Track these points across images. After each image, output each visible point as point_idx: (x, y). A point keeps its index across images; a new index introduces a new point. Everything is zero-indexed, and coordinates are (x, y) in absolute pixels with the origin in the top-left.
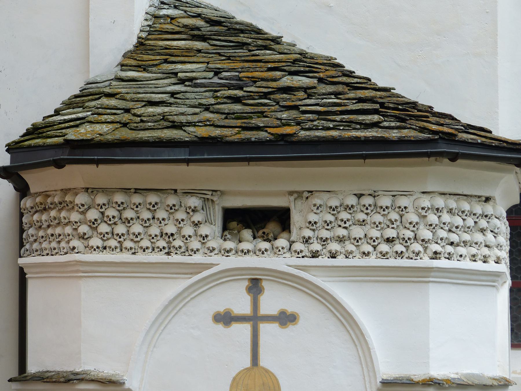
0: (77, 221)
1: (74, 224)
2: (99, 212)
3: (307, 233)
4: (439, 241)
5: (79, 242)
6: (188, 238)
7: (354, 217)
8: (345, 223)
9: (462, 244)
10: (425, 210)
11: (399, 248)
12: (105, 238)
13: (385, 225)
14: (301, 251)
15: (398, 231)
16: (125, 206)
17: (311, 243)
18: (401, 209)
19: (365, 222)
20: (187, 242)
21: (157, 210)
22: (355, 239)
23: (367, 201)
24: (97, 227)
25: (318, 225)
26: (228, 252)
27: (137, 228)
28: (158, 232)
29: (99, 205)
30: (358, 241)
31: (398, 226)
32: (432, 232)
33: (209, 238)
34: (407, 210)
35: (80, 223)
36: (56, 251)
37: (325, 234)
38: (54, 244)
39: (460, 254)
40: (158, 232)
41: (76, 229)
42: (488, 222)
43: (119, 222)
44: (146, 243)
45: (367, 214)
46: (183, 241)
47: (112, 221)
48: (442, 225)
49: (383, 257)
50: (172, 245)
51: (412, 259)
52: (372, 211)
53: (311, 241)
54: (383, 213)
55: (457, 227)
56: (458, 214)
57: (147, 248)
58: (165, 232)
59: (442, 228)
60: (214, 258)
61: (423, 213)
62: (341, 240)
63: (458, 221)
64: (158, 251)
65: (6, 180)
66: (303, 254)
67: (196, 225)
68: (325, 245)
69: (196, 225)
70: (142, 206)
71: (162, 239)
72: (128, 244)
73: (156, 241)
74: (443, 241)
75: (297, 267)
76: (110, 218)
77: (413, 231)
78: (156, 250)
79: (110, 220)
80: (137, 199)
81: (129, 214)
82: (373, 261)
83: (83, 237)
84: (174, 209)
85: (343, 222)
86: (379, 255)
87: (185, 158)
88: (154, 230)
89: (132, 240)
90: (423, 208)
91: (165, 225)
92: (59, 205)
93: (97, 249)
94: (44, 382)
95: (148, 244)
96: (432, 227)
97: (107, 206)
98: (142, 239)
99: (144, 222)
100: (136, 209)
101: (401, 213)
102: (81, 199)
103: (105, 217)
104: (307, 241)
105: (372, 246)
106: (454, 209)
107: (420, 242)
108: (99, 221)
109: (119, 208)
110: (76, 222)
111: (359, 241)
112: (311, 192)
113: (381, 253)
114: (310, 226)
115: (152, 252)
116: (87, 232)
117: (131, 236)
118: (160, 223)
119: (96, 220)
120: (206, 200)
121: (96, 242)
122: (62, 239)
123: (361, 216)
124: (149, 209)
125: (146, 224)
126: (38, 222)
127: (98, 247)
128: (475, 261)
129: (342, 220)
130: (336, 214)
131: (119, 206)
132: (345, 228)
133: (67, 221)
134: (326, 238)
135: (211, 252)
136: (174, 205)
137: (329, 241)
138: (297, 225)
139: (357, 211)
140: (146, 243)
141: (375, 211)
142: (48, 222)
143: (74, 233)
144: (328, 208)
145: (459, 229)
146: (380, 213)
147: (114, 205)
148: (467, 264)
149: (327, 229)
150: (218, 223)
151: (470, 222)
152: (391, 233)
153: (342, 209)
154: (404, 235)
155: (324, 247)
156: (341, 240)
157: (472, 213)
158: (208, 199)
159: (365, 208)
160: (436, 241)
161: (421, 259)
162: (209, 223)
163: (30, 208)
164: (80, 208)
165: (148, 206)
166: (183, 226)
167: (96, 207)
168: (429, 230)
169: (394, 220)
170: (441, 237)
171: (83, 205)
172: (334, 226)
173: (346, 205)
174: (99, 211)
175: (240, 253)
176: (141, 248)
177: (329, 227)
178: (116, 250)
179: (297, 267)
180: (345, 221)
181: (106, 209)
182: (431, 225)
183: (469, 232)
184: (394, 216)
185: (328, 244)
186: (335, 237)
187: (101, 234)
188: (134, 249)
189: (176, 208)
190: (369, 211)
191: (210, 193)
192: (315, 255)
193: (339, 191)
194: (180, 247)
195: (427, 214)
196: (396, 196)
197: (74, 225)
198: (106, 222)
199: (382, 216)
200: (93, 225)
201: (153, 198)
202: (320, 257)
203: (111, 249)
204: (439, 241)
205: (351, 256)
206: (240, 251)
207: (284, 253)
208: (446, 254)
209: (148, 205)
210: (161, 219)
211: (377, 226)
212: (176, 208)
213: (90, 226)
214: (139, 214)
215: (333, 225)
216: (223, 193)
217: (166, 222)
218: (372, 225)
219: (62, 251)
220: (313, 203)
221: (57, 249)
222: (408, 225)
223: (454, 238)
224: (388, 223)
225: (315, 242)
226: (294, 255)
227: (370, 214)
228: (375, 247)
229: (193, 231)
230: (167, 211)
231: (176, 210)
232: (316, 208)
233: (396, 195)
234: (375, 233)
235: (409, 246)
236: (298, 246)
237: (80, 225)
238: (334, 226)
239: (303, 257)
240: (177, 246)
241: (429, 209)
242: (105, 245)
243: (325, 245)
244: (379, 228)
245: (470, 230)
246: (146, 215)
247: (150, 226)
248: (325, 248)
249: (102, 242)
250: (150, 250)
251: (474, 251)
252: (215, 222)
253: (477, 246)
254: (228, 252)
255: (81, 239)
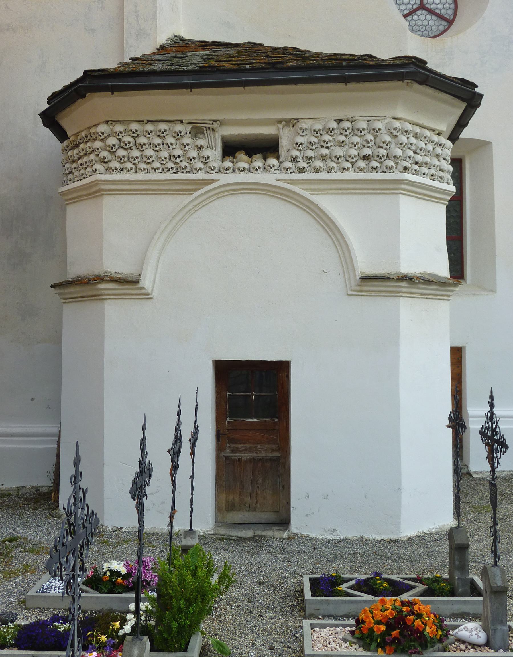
0: (98, 147)
1: (97, 150)
2: (116, 139)
3: (295, 153)
4: (408, 159)
5: (101, 165)
6: (192, 160)
7: (334, 139)
8: (327, 143)
9: (424, 165)
10: (397, 130)
11: (375, 164)
12: (122, 161)
13: (361, 145)
14: (290, 168)
15: (373, 151)
16: (139, 133)
17: (298, 162)
18: (375, 131)
19: (344, 143)
20: (192, 162)
21: (166, 137)
22: (336, 157)
23: (346, 125)
24: (115, 152)
25: (304, 146)
26: (227, 169)
27: (149, 152)
28: (166, 155)
29: (116, 133)
30: (338, 159)
31: (372, 145)
32: (402, 150)
33: (210, 159)
34: (381, 132)
35: (101, 149)
36: (84, 176)
37: (310, 153)
38: (82, 171)
39: (423, 172)
40: (166, 155)
41: (98, 155)
42: (442, 150)
43: (134, 148)
44: (156, 165)
45: (346, 136)
46: (188, 163)
47: (127, 145)
48: (410, 146)
49: (360, 172)
50: (179, 165)
51: (385, 172)
52: (350, 133)
53: (298, 160)
54: (359, 134)
55: (421, 150)
56: (421, 139)
57: (158, 169)
58: (172, 155)
59: (409, 148)
60: (214, 176)
61: (395, 133)
62: (323, 158)
63: (422, 145)
64: (167, 171)
65: (48, 128)
66: (292, 171)
67: (199, 148)
68: (310, 163)
69: (199, 148)
70: (153, 134)
71: (170, 161)
72: (142, 166)
73: (165, 163)
74: (411, 159)
75: (285, 181)
76: (126, 144)
77: (386, 149)
78: (165, 170)
79: (126, 145)
80: (149, 127)
81: (142, 140)
82: (350, 175)
83: (104, 161)
84: (180, 135)
85: (326, 143)
86: (357, 170)
87: (188, 82)
88: (164, 154)
89: (145, 162)
90: (395, 129)
91: (173, 149)
92: (85, 138)
93: (115, 170)
94: (76, 284)
95: (159, 165)
96: (403, 146)
97: (123, 134)
98: (153, 161)
99: (154, 147)
100: (148, 136)
101: (376, 134)
102: (103, 128)
103: (122, 143)
104: (294, 160)
105: (351, 163)
106: (418, 133)
107: (393, 159)
108: (117, 147)
109: (133, 135)
110: (98, 149)
111: (340, 159)
112: (297, 119)
113: (358, 168)
114: (297, 147)
115: (161, 172)
116: (107, 156)
117: (145, 159)
118: (169, 147)
119: (114, 145)
120: (208, 128)
121: (115, 164)
122: (88, 166)
123: (342, 138)
124: (159, 136)
125: (156, 149)
126: (71, 156)
127: (116, 169)
128: (433, 180)
129: (324, 141)
130: (319, 136)
131: (133, 133)
132: (327, 148)
133: (91, 149)
134: (311, 157)
135: (212, 170)
136: (180, 132)
137: (313, 160)
138: (285, 148)
139: (337, 134)
140: (156, 165)
141: (352, 134)
142: (78, 155)
143: (97, 159)
144: (312, 131)
145: (422, 151)
146: (357, 135)
147: (129, 132)
148: (427, 181)
149: (311, 149)
150: (218, 149)
151: (430, 147)
152: (367, 152)
153: (325, 132)
154: (378, 152)
155: (309, 164)
156: (323, 158)
157: (430, 140)
158: (209, 128)
159: (345, 130)
160: (405, 159)
161: (393, 172)
162: (210, 148)
163: (66, 147)
164: (100, 136)
165: (158, 133)
166: (188, 149)
167: (115, 135)
168: (399, 148)
169: (369, 140)
170: (409, 155)
171: (103, 133)
172: (318, 147)
173: (327, 129)
174: (117, 139)
175: (237, 171)
176: (152, 168)
177: (313, 147)
178: (131, 171)
179: (285, 181)
180: (327, 142)
181: (122, 137)
182: (401, 144)
183: (429, 155)
184: (370, 137)
185: (312, 162)
186: (318, 157)
187: (118, 157)
188: (146, 170)
189: (182, 134)
190: (347, 133)
191: (211, 122)
192: (302, 170)
193: (321, 118)
194: (186, 167)
195: (382, 160)
196: (370, 122)
197: (96, 152)
198: (122, 148)
199: (359, 137)
200: (112, 149)
201: (163, 126)
202: (306, 173)
203: (127, 170)
204: (408, 159)
205: (333, 171)
206: (237, 169)
207: (275, 170)
208: (413, 170)
209: (158, 132)
210: (169, 144)
211: (355, 146)
212: (182, 134)
213: (109, 151)
214: (150, 141)
215: (316, 146)
216: (222, 123)
217: (174, 146)
218: (350, 145)
219: (87, 175)
220: (300, 127)
221: (84, 175)
222: (382, 144)
223: (419, 158)
224: (365, 143)
225: (301, 160)
226: (283, 171)
227: (348, 136)
228: (353, 164)
229: (197, 154)
230: (175, 137)
231: (182, 136)
232: (302, 131)
233: (370, 120)
234: (354, 152)
235: (382, 163)
236: (288, 164)
237: (101, 151)
238: (318, 147)
239: (291, 173)
240: (183, 166)
241: (400, 130)
242: (122, 167)
243: (310, 163)
244: (356, 148)
245: (430, 153)
246: (158, 141)
247: (160, 150)
248: (310, 166)
249: (119, 164)
250: (160, 170)
251: (433, 171)
252: (215, 147)
253: (435, 168)
254: (227, 169)
255: (102, 163)
